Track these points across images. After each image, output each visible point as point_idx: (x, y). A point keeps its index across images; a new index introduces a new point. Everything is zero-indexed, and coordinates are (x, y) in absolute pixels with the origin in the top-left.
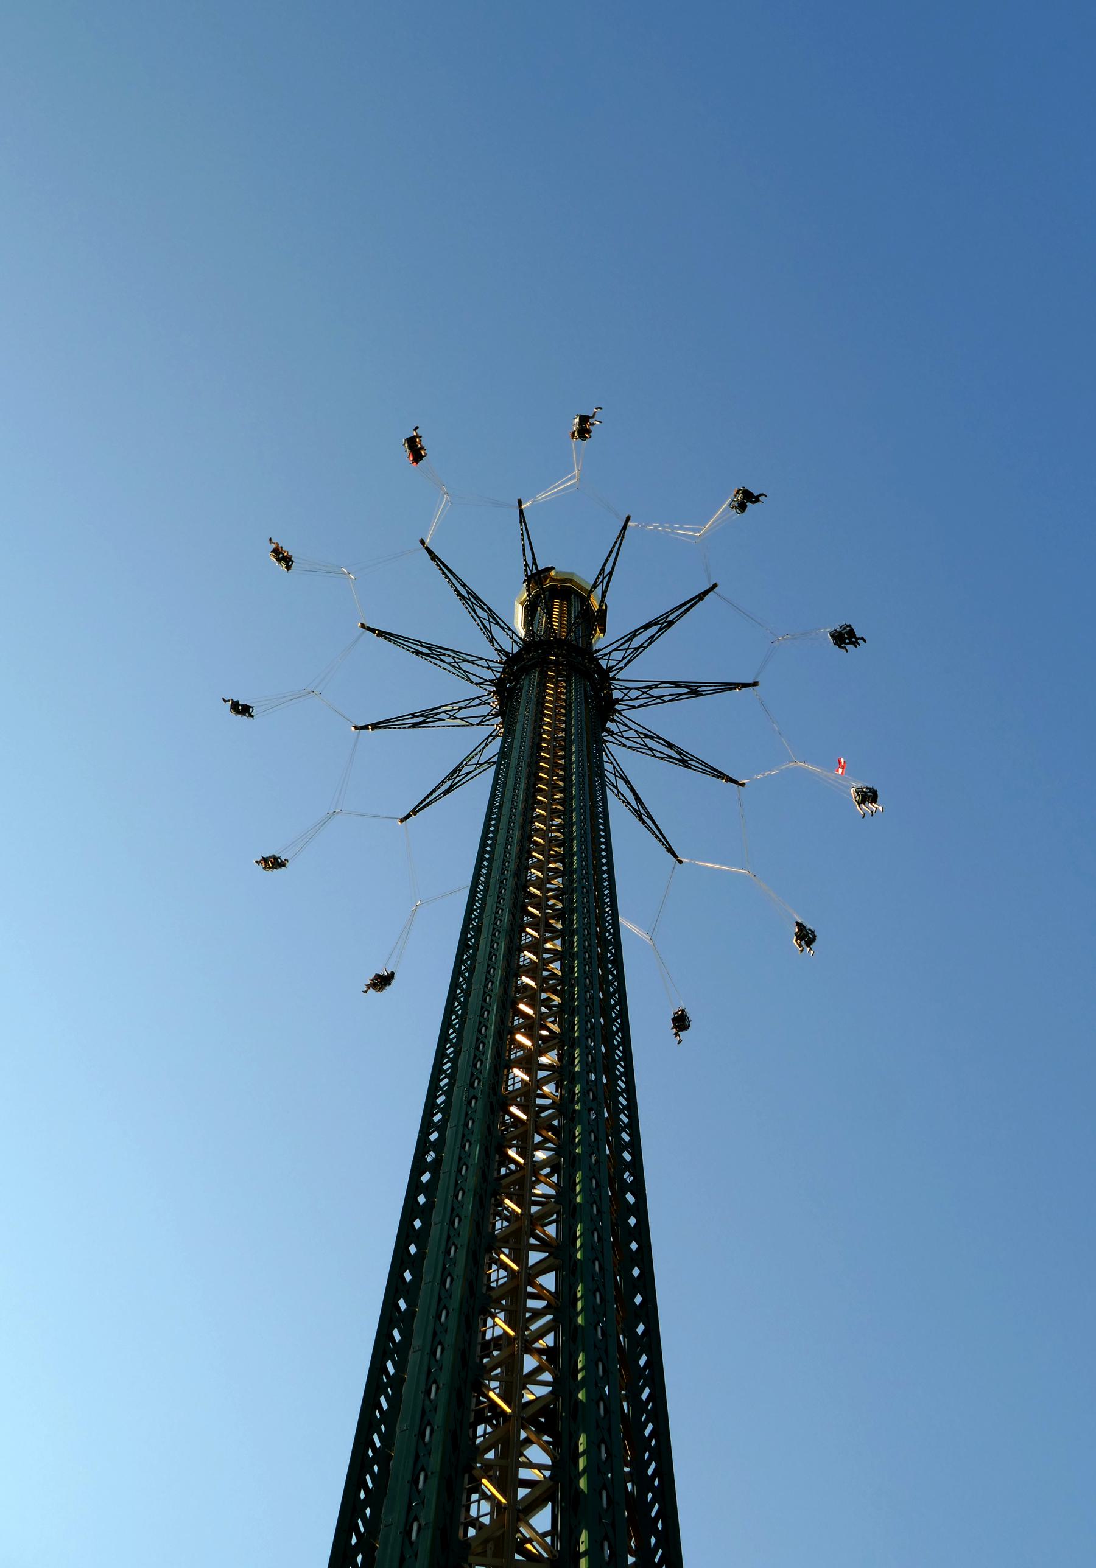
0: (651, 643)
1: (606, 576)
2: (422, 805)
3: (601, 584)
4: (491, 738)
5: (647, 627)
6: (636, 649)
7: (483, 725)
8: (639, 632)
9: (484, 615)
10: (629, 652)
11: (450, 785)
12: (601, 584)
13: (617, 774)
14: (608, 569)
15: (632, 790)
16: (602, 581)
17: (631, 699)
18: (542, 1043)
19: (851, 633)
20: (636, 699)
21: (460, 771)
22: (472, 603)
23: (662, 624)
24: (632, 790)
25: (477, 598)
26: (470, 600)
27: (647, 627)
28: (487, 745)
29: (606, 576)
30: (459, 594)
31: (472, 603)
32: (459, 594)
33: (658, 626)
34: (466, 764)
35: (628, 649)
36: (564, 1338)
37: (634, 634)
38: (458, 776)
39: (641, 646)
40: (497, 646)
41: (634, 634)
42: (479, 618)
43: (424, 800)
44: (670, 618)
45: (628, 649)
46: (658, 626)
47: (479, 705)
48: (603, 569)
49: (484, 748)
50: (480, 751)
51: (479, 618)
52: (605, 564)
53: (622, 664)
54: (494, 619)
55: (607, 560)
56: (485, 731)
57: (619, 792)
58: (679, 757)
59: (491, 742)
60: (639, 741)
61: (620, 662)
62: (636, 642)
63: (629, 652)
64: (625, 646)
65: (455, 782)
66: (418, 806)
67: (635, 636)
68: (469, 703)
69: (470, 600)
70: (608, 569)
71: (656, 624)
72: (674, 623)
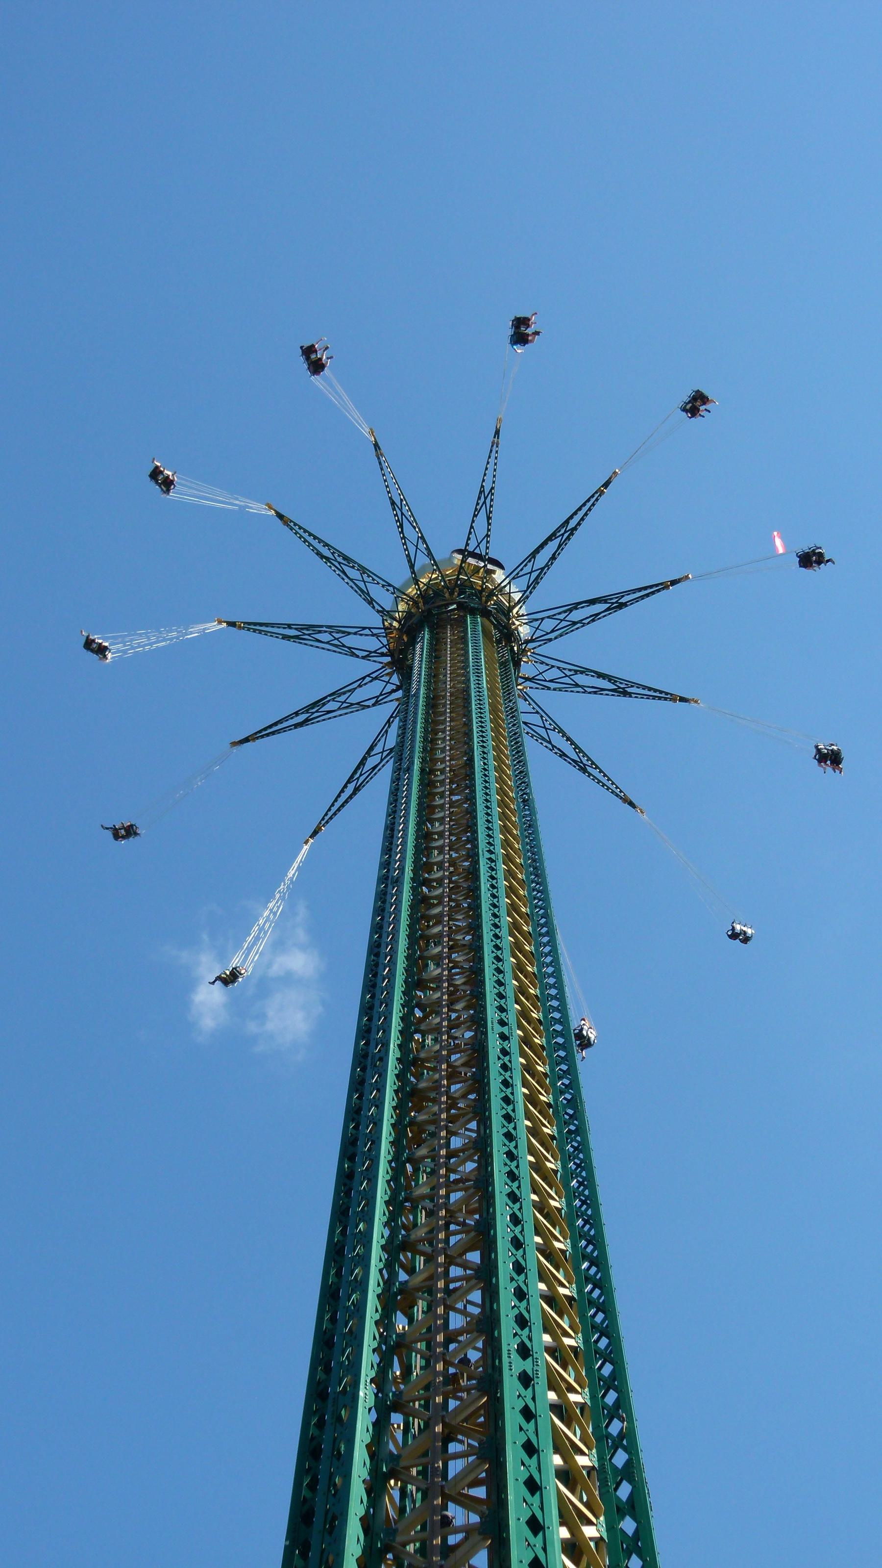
0: (593, 620)
1: (568, 531)
2: (266, 732)
3: (561, 537)
4: (368, 679)
5: (592, 602)
6: (574, 623)
7: (369, 660)
8: (582, 606)
9: (354, 574)
10: (564, 624)
11: (305, 718)
12: (561, 537)
13: (568, 673)
14: (572, 524)
15: (600, 675)
16: (563, 535)
17: (545, 681)
18: (420, 934)
19: (116, 836)
20: (553, 631)
21: (324, 704)
22: (309, 635)
23: (613, 603)
24: (600, 675)
25: (309, 627)
26: (305, 634)
27: (592, 602)
28: (360, 686)
29: (568, 531)
30: (322, 557)
31: (309, 635)
32: (322, 557)
33: (608, 605)
34: (333, 700)
35: (564, 620)
36: (556, 1354)
37: (576, 606)
38: (317, 711)
39: (580, 621)
40: (377, 607)
41: (576, 606)
42: (351, 580)
43: (270, 726)
44: (623, 600)
45: (564, 620)
46: (608, 605)
47: (371, 681)
48: (567, 522)
49: (349, 633)
50: (349, 691)
51: (351, 580)
52: (571, 517)
53: (552, 636)
54: (338, 632)
55: (575, 513)
56: (370, 667)
57: (582, 687)
58: (386, 773)
59: (365, 684)
60: (567, 680)
61: (548, 634)
62: (576, 616)
63: (564, 624)
64: (562, 617)
65: (311, 717)
66: (260, 732)
67: (576, 608)
68: (360, 631)
69: (305, 634)
70: (572, 524)
71: (606, 602)
72: (626, 606)
